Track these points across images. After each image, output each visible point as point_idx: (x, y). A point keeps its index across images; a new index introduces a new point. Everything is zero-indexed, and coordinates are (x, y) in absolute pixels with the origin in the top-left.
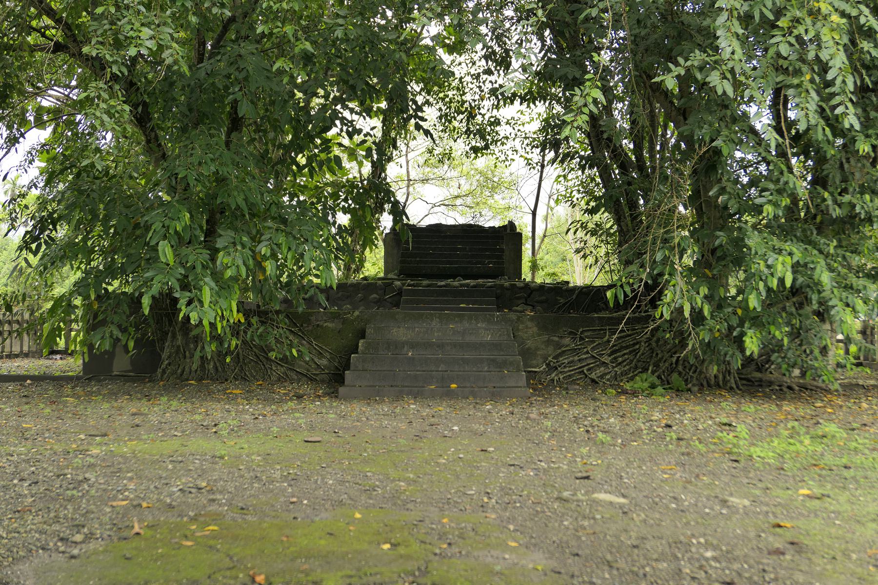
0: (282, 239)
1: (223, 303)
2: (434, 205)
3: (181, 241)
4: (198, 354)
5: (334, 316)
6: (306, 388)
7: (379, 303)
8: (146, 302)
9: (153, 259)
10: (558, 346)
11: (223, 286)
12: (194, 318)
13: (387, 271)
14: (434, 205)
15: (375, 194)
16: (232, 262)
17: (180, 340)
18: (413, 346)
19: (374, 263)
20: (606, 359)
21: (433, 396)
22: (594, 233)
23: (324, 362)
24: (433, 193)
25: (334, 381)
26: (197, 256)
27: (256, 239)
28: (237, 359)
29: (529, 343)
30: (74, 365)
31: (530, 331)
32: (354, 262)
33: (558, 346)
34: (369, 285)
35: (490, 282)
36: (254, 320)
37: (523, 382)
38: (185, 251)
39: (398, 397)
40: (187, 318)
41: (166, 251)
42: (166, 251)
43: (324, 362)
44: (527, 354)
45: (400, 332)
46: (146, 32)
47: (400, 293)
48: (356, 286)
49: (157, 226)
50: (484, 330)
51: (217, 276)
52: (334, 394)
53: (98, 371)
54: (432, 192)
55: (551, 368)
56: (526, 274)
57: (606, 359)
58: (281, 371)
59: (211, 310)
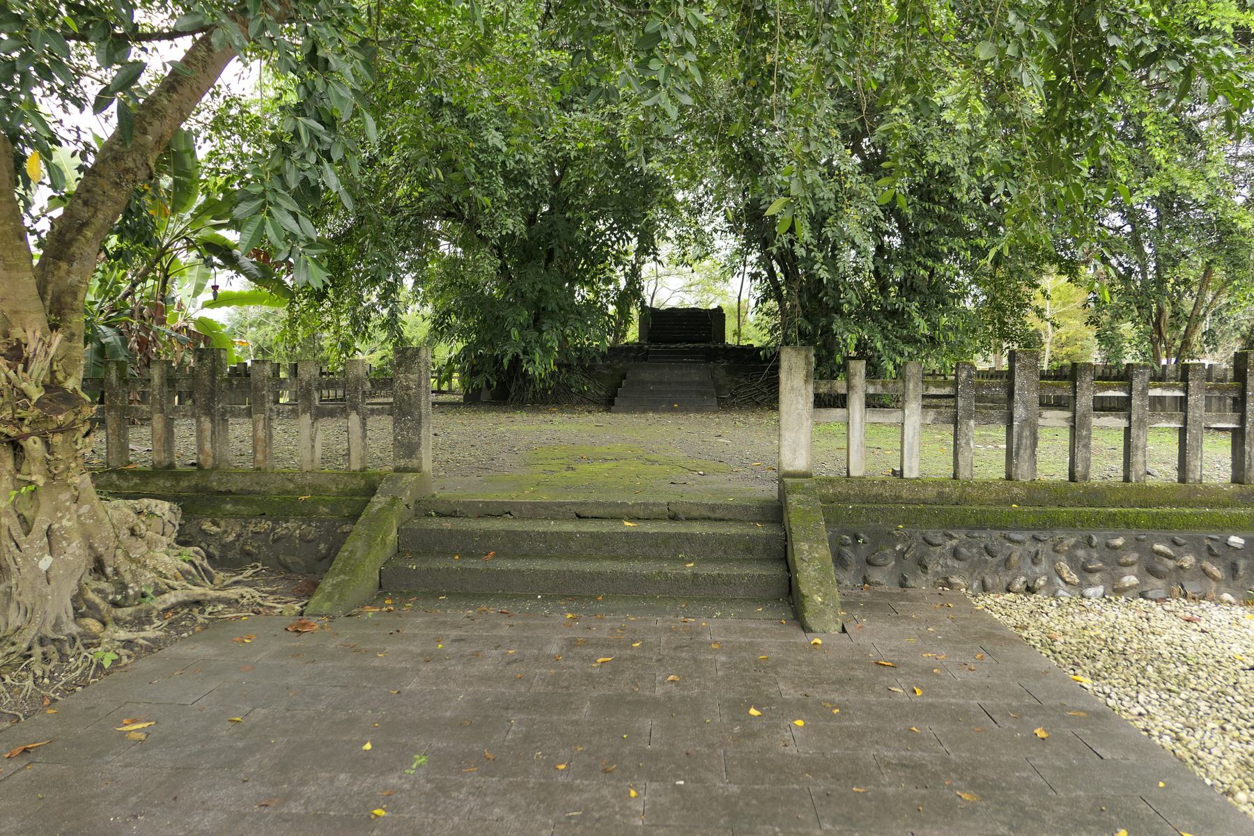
0: (578, 325)
1: (546, 361)
2: (675, 291)
3: (522, 328)
4: (531, 389)
5: (608, 367)
6: (593, 407)
7: (635, 358)
8: (505, 361)
9: (508, 337)
10: (738, 383)
11: (547, 351)
12: (530, 370)
13: (640, 338)
14: (675, 291)
15: (633, 292)
16: (551, 339)
17: (521, 381)
18: (653, 383)
19: (633, 334)
20: (765, 390)
21: (664, 411)
22: (767, 314)
23: (602, 393)
24: (675, 282)
25: (608, 404)
26: (532, 335)
27: (564, 324)
28: (553, 393)
29: (721, 382)
30: (459, 398)
31: (721, 374)
32: (620, 332)
33: (738, 383)
34: (629, 347)
35: (702, 345)
36: (564, 370)
37: (715, 403)
38: (525, 332)
39: (645, 411)
40: (527, 370)
41: (515, 333)
42: (515, 333)
43: (602, 393)
44: (719, 388)
45: (646, 376)
46: (510, 221)
47: (648, 352)
48: (622, 349)
49: (510, 319)
50: (695, 374)
51: (543, 346)
52: (608, 410)
53: (472, 400)
54: (669, 288)
55: (733, 396)
56: (730, 340)
57: (765, 390)
58: (578, 398)
59: (539, 367)
